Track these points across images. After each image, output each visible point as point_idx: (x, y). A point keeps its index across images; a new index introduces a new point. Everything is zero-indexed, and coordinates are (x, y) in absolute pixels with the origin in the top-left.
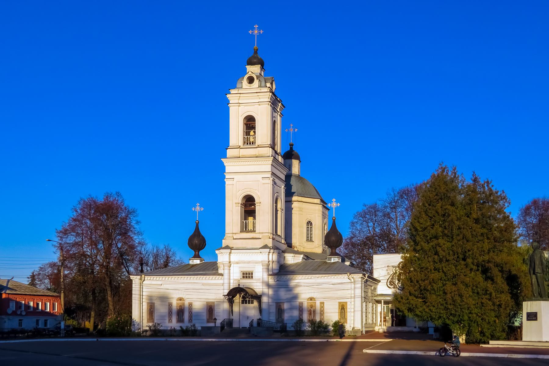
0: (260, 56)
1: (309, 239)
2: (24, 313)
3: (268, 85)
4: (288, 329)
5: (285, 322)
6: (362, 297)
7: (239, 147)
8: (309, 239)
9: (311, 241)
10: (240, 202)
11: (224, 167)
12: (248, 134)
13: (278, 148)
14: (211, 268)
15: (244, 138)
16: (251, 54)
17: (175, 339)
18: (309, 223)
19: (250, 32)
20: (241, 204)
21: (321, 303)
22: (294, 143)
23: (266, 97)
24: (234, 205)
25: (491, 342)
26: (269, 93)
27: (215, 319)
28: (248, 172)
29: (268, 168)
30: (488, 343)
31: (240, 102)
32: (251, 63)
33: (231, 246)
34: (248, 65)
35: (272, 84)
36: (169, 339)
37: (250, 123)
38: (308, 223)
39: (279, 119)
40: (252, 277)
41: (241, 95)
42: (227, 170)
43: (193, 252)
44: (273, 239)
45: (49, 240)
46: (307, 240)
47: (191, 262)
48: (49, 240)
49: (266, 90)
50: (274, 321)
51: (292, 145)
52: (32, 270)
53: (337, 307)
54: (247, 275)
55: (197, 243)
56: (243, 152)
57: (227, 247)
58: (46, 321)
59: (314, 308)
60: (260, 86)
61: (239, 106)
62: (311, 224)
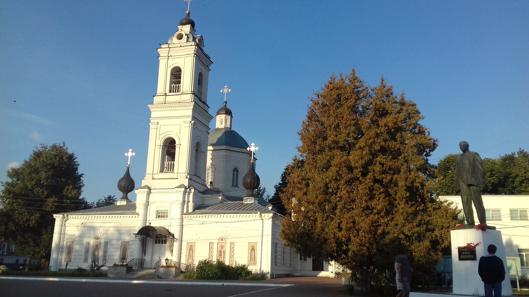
0: (192, 18)
2: (5, 254)
11: (150, 113)
15: (170, 86)
16: (185, 16)
17: (84, 280)
18: (236, 170)
29: (190, 112)
32: (183, 24)
37: (176, 74)
42: (153, 115)
46: (233, 185)
54: (160, 215)
59: (224, 249)
60: (187, 41)
62: (237, 171)
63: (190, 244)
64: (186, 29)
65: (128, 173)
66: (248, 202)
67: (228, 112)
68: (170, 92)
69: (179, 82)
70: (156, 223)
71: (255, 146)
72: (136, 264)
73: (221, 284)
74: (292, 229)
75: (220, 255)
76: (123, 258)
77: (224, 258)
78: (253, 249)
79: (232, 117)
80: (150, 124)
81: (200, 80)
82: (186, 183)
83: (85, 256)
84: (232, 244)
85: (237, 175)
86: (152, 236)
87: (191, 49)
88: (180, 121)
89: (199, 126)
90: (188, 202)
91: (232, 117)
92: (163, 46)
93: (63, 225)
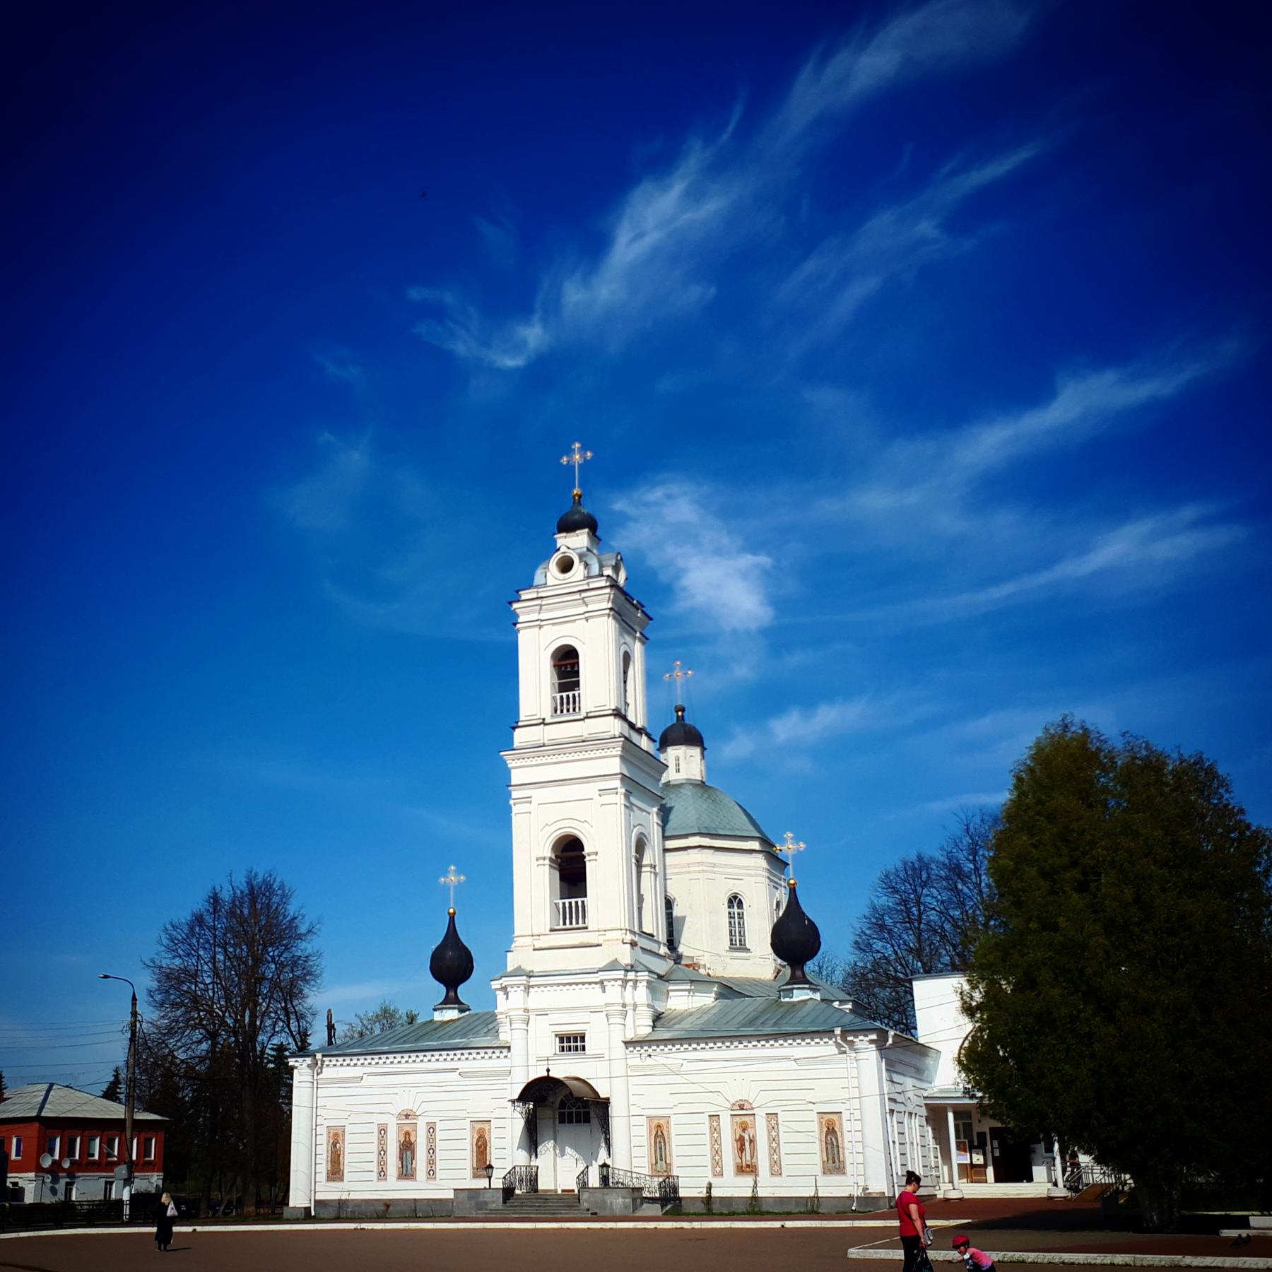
1: (738, 944)
3: (608, 571)
4: (683, 1193)
5: (675, 1172)
6: (882, 1095)
7: (543, 723)
8: (738, 944)
9: (743, 948)
10: (548, 853)
11: (507, 772)
12: (563, 688)
13: (637, 715)
14: (478, 1031)
18: (735, 901)
19: (564, 460)
20: (551, 859)
22: (685, 705)
23: (602, 601)
24: (535, 863)
26: (608, 590)
27: (490, 1167)
28: (562, 783)
30: (1243, 1223)
31: (542, 616)
32: (568, 526)
33: (528, 967)
34: (560, 531)
35: (616, 569)
36: (789, 1224)
37: (566, 663)
38: (730, 901)
40: (584, 1048)
41: (545, 602)
42: (516, 777)
43: (441, 990)
45: (106, 977)
46: (733, 947)
47: (438, 1017)
48: (106, 977)
49: (602, 582)
50: (646, 1171)
51: (683, 710)
52: (113, 1067)
54: (572, 1042)
55: (452, 966)
57: (518, 972)
59: (751, 1131)
61: (540, 627)
62: (740, 904)
63: (656, 1122)
64: (576, 541)
65: (452, 932)
66: (795, 999)
67: (692, 737)
70: (563, 1069)
71: (796, 840)
73: (777, 1224)
75: (742, 1149)
76: (484, 1167)
77: (752, 1158)
78: (831, 1133)
80: (511, 802)
83: (379, 1163)
84: (431, 1128)
85: (741, 916)
88: (592, 789)
90: (635, 1006)
91: (704, 749)
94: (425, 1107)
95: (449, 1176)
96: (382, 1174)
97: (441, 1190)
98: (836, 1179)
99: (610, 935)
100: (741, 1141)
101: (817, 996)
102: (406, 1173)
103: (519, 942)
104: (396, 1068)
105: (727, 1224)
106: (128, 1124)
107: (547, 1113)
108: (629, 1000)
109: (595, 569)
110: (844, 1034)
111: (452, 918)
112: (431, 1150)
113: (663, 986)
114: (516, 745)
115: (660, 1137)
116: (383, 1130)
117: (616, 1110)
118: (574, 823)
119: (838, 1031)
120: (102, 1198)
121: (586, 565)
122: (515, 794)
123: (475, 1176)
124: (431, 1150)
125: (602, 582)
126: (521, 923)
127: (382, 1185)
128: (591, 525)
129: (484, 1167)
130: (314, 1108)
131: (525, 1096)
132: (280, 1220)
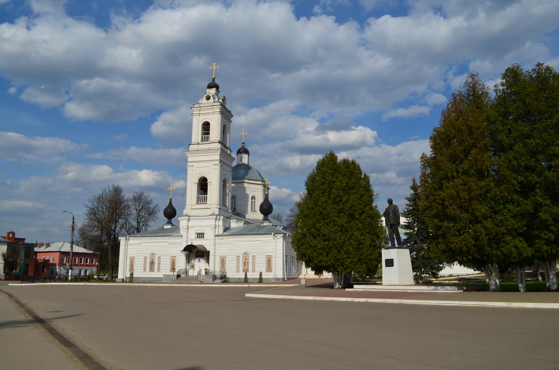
0: (217, 82)
7: (198, 144)
10: (197, 182)
15: (202, 137)
16: (210, 81)
19: (210, 68)
21: (254, 256)
25: (355, 286)
29: (217, 157)
33: (189, 214)
36: (251, 285)
37: (206, 127)
39: (414, 137)
42: (190, 159)
44: (220, 208)
47: (165, 227)
49: (218, 104)
53: (265, 259)
54: (200, 235)
56: (201, 147)
57: (186, 215)
58: (86, 271)
64: (213, 91)
65: (171, 203)
68: (202, 140)
69: (208, 134)
70: (197, 242)
72: (183, 273)
73: (247, 285)
74: (480, 92)
75: (245, 265)
76: (173, 269)
79: (249, 155)
81: (224, 130)
82: (217, 212)
84: (159, 258)
86: (194, 252)
87: (218, 109)
88: (211, 164)
89: (224, 167)
90: (219, 226)
91: (249, 155)
92: (196, 106)
93: (126, 245)
94: (157, 252)
95: (164, 271)
96: (145, 270)
97: (159, 275)
98: (269, 273)
99: (213, 206)
100: (245, 263)
101: (271, 224)
102: (152, 270)
103: (187, 207)
104: (152, 241)
105: (180, 285)
106: (71, 254)
107: (193, 255)
108: (217, 224)
109: (217, 100)
110: (275, 234)
111: (171, 200)
112: (159, 264)
113: (228, 220)
114: (190, 150)
115: (223, 261)
116: (145, 258)
117: (211, 254)
118: (205, 173)
119: (273, 233)
120: (259, 277)
121: (214, 99)
122: (189, 164)
123: (171, 271)
124: (159, 264)
125: (218, 104)
126: (188, 202)
127: (238, 273)
128: (217, 87)
129: (173, 269)
130: (126, 252)
131: (185, 250)
132: (115, 282)
